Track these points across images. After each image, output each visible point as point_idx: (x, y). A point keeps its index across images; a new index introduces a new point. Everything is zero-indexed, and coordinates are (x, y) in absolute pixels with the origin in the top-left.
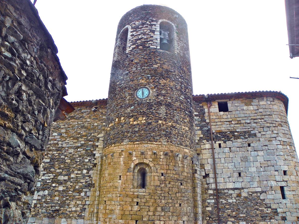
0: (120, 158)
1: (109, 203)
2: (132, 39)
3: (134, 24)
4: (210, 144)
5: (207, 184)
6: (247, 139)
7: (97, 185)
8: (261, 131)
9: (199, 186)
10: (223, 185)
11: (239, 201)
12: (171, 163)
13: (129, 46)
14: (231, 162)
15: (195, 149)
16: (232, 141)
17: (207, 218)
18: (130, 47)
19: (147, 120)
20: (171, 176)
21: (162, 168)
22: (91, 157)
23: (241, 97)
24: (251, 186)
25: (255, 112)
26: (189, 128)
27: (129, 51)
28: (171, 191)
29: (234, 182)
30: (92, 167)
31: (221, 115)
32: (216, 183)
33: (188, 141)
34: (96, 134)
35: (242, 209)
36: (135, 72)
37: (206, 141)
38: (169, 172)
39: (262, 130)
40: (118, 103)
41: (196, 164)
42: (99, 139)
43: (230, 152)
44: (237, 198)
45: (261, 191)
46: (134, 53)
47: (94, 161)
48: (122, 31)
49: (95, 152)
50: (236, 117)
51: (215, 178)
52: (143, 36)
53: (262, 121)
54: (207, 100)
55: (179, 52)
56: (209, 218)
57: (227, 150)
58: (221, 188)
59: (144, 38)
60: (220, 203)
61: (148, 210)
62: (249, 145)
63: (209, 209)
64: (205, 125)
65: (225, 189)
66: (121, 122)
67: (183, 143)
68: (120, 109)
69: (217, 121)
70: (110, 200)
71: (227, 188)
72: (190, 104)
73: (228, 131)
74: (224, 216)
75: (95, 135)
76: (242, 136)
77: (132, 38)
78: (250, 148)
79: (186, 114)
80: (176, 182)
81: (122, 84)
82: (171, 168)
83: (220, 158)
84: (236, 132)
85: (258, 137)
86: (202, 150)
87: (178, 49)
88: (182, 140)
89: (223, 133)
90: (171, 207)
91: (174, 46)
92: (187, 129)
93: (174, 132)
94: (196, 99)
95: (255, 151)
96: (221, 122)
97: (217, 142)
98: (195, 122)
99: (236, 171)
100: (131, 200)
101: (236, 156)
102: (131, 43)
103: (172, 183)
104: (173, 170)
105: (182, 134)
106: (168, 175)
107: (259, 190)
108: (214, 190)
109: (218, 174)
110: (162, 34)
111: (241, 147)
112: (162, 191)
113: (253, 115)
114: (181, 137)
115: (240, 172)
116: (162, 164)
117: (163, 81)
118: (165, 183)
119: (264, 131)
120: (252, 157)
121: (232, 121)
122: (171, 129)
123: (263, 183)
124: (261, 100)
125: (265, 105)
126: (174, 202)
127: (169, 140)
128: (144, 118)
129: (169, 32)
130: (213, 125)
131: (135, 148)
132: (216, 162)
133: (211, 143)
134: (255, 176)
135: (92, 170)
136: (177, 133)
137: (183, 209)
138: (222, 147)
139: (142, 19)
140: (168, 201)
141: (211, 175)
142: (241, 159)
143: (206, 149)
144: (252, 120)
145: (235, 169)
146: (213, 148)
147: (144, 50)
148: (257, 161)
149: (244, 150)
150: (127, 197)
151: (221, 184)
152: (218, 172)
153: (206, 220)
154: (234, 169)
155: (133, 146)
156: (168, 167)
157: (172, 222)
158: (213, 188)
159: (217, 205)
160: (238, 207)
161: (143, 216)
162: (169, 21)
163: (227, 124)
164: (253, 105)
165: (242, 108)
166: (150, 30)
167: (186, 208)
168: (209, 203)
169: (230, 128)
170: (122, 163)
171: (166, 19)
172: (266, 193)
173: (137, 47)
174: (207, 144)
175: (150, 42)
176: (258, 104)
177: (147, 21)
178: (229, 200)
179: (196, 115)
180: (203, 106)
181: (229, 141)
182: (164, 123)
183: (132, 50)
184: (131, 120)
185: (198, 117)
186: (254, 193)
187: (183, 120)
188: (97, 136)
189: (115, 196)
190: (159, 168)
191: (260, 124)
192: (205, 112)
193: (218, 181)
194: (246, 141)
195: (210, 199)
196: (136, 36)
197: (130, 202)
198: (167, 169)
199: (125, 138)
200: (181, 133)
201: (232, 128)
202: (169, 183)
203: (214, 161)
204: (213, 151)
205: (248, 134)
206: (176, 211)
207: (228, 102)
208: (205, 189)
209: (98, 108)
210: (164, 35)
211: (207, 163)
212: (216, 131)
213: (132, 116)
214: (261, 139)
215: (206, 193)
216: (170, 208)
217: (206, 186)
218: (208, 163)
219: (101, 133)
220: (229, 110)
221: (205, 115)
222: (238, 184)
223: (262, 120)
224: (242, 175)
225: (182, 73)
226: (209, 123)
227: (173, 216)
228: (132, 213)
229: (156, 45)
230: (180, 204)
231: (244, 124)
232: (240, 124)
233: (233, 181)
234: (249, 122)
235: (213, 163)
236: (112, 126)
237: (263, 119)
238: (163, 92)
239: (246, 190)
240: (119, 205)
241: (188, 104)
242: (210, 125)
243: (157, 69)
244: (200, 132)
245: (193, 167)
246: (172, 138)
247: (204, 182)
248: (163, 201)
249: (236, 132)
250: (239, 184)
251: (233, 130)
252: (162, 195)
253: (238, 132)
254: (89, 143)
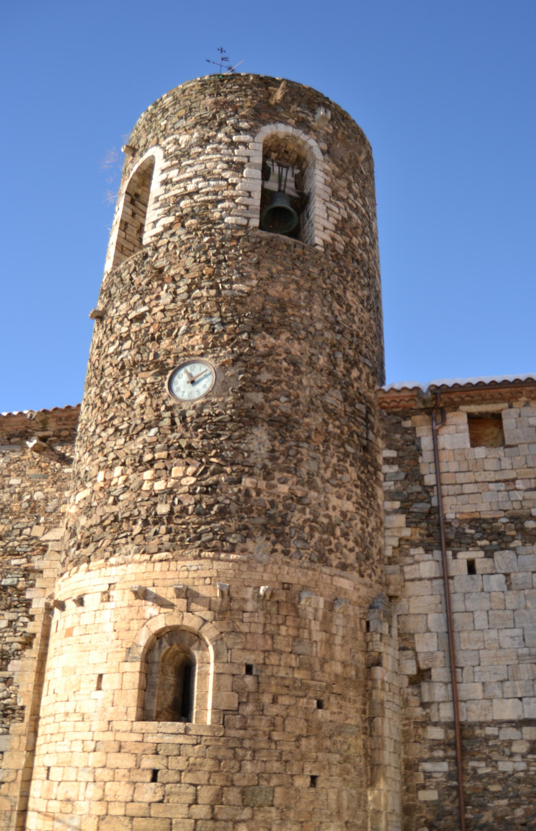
4: (438, 561)
5: (424, 705)
7: (27, 712)
9: (388, 713)
10: (479, 707)
14: (508, 626)
16: (514, 549)
18: (155, 222)
19: (202, 473)
20: (282, 673)
21: (248, 646)
22: (17, 610)
26: (359, 503)
28: (280, 728)
29: (520, 699)
30: (19, 646)
31: (477, 457)
32: (455, 701)
33: (351, 550)
34: (37, 531)
37: (421, 550)
38: (274, 659)
40: (109, 418)
41: (381, 634)
42: (46, 546)
46: (169, 242)
47: (25, 625)
54: (429, 405)
58: (473, 718)
61: (190, 799)
65: (489, 724)
68: (112, 438)
69: (464, 481)
72: (366, 420)
73: (502, 514)
74: (484, 820)
75: (33, 534)
79: (347, 454)
81: (125, 350)
82: (281, 644)
83: (472, 612)
86: (408, 584)
87: (325, 228)
89: (485, 521)
90: (278, 790)
92: (349, 506)
93: (297, 518)
96: (476, 482)
97: (460, 555)
98: (385, 484)
104: (291, 653)
106: (268, 671)
114: (325, 536)
118: (258, 701)
127: (279, 547)
128: (191, 470)
129: (298, 168)
131: (153, 576)
132: (457, 627)
136: (309, 520)
137: (323, 798)
138: (477, 572)
139: (202, 122)
140: (268, 765)
143: (420, 579)
145: (525, 651)
147: (203, 231)
150: (119, 751)
151: (473, 706)
152: (461, 662)
154: (520, 651)
155: (150, 566)
156: (270, 642)
159: (457, 780)
161: (174, 822)
163: (498, 491)
167: (336, 790)
168: (428, 775)
169: (507, 506)
173: (182, 220)
175: (226, 204)
177: (217, 131)
179: (388, 461)
180: (414, 429)
181: (502, 549)
182: (262, 484)
184: (148, 475)
185: (395, 468)
187: (333, 476)
188: (43, 539)
189: (80, 749)
190: (236, 647)
193: (462, 694)
196: (178, 182)
197: (130, 770)
198: (268, 647)
199: (123, 541)
200: (325, 521)
201: (517, 505)
202: (274, 701)
203: (450, 622)
204: (446, 586)
208: (415, 723)
209: (51, 441)
210: (280, 182)
211: (424, 629)
213: (152, 463)
216: (274, 791)
217: (419, 711)
218: (428, 631)
219: (56, 527)
221: (420, 460)
225: (339, 311)
228: (133, 812)
230: (314, 779)
235: (444, 629)
238: (265, 377)
240: (91, 779)
241: (359, 419)
243: (246, 298)
244: (400, 520)
245: (367, 643)
247: (411, 698)
248: (248, 767)
251: (521, 511)
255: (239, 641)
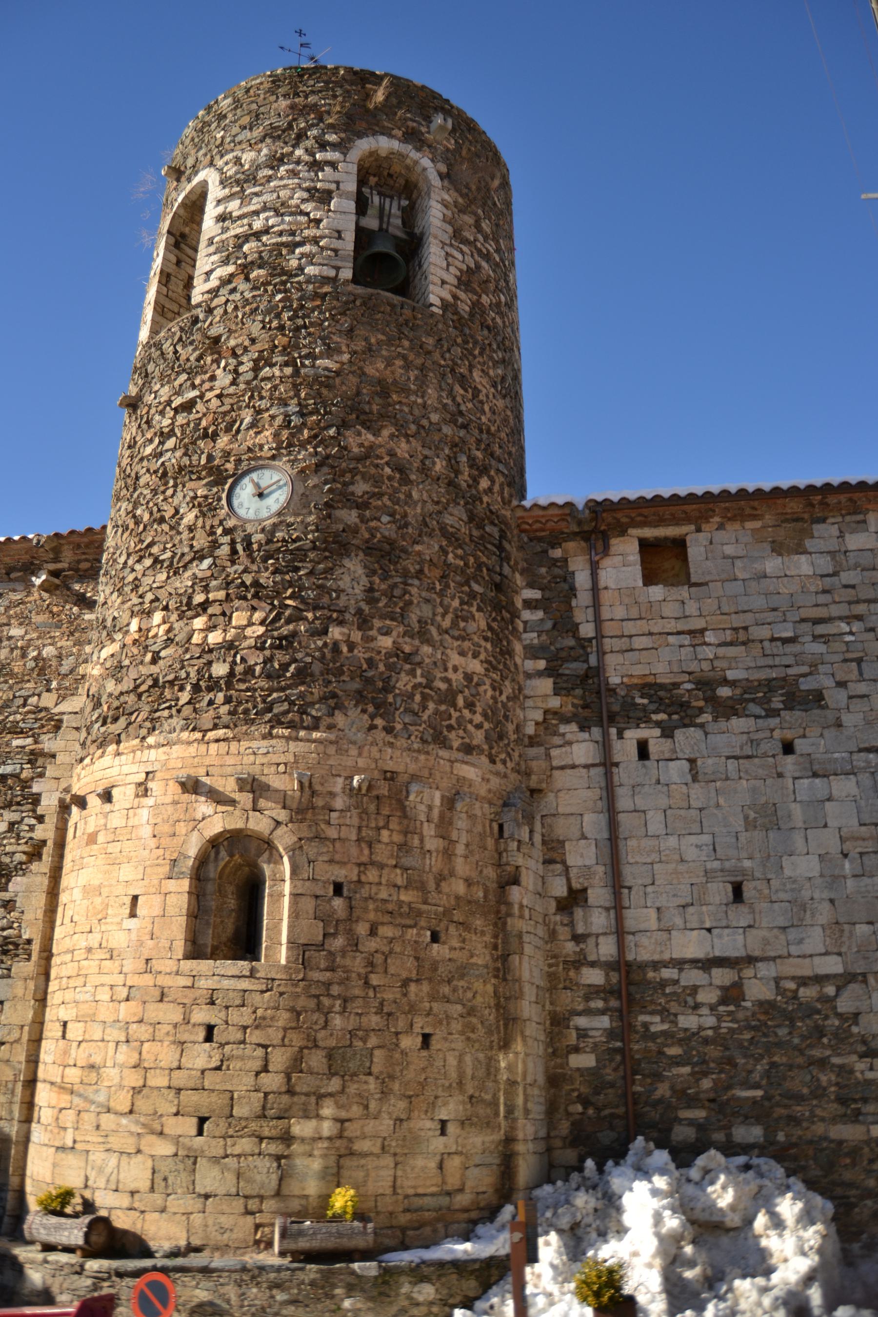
0: (139, 811)
1: (81, 1032)
2: (224, 236)
3: (238, 161)
4: (597, 742)
5: (577, 938)
6: (779, 715)
8: (846, 679)
10: (653, 941)
11: (730, 1025)
12: (385, 833)
13: (208, 268)
15: (518, 764)
16: (702, 726)
17: (571, 1109)
18: (208, 274)
19: (274, 621)
20: (383, 895)
21: (337, 857)
22: (20, 808)
23: (755, 512)
24: (794, 950)
25: (820, 584)
27: (203, 294)
28: (380, 969)
29: (709, 930)
30: (24, 858)
31: (652, 599)
32: (620, 932)
33: (479, 727)
34: (48, 700)
35: (746, 1064)
36: (225, 392)
37: (574, 727)
39: (855, 675)
40: (145, 544)
41: (519, 841)
42: (61, 721)
43: (695, 779)
44: (721, 1008)
45: (841, 975)
47: (32, 828)
48: (180, 199)
49: (42, 784)
50: (725, 609)
51: (618, 908)
52: (271, 217)
53: (854, 630)
55: (449, 298)
56: (579, 1108)
57: (677, 771)
58: (644, 956)
59: (276, 229)
60: (637, 1032)
61: (257, 1065)
62: (788, 748)
63: (585, 1061)
64: (572, 648)
65: (665, 964)
66: (151, 634)
67: (452, 735)
69: (633, 633)
70: (83, 1016)
71: (674, 956)
73: (686, 677)
74: (658, 1094)
76: (753, 700)
77: (223, 228)
78: (790, 759)
79: (473, 595)
80: (410, 927)
81: (167, 451)
82: (382, 854)
83: (644, 812)
84: (725, 682)
85: (831, 704)
86: (556, 773)
87: (443, 282)
88: (448, 722)
89: (662, 687)
90: (377, 1052)
91: (425, 266)
92: (476, 666)
94: (534, 527)
95: (815, 775)
96: (651, 634)
97: (628, 734)
98: (525, 636)
99: (719, 874)
100: (178, 1017)
101: (721, 801)
102: (215, 258)
103: (386, 931)
104: (396, 866)
105: (450, 689)
107: (833, 966)
108: (610, 966)
109: (630, 888)
110: (369, 212)
111: (748, 757)
112: (332, 969)
113: (813, 600)
114: (443, 708)
115: (739, 879)
116: (336, 836)
117: (359, 434)
118: (350, 932)
119: (866, 676)
120: (798, 805)
121: (705, 629)
122: (390, 667)
123: (851, 932)
124: (854, 525)
125: (871, 550)
126: (395, 1026)
127: (379, 722)
128: (258, 616)
130: (612, 652)
131: (207, 761)
132: (623, 832)
133: (600, 739)
134: (812, 899)
135: (21, 872)
138: (651, 757)
140: (364, 1019)
141: (598, 895)
142: (746, 818)
143: (573, 767)
144: (806, 627)
145: (716, 865)
146: (608, 764)
147: (275, 285)
148: (825, 826)
149: (761, 772)
150: (161, 1001)
151: (644, 940)
153: (569, 1114)
154: (709, 865)
155: (203, 748)
156: (366, 852)
157: (381, 1124)
158: (603, 959)
159: (622, 1041)
160: (727, 1053)
161: (236, 1096)
162: (408, 149)
163: (681, 646)
164: (810, 553)
165: (758, 566)
166: (308, 190)
167: (457, 1053)
168: (583, 1033)
169: (693, 666)
170: (146, 832)
171: (391, 136)
172: (865, 981)
174: (577, 741)
175: (307, 248)
176: (839, 543)
177: (295, 146)
178: (681, 1018)
179: (529, 604)
180: (565, 560)
181: (685, 726)
183: (218, 291)
184: (199, 623)
185: (540, 614)
186: (805, 984)
188: (56, 710)
189: (107, 997)
190: (320, 859)
191: (847, 643)
192: (577, 585)
193: (630, 923)
194: (772, 726)
195: (588, 1012)
196: (240, 218)
197: (175, 1026)
198: (364, 859)
199: (166, 713)
200: (443, 686)
201: (706, 666)
202: (373, 932)
203: (613, 825)
204: (608, 776)
205: (782, 695)
206: (401, 1071)
207: (688, 538)
209: (65, 576)
210: (381, 218)
211: (578, 834)
212: (625, 680)
213: (204, 606)
214: (847, 719)
215: (571, 986)
216: (372, 1055)
217: (570, 947)
218: (584, 837)
219: (72, 695)
220: (694, 579)
221: (574, 603)
222: (726, 939)
223: (856, 626)
224: (748, 891)
226: (594, 641)
227: (385, 1093)
229: (334, 263)
230: (426, 1039)
231: (766, 644)
232: (744, 643)
233: (703, 922)
234: (789, 634)
235: (606, 835)
236: (112, 655)
237: (859, 618)
239: (766, 970)
240: (123, 1039)
241: (489, 546)
242: (598, 651)
243: (334, 378)
244: (546, 685)
245: (500, 854)
246: (392, 709)
247: (560, 929)
248: (337, 1021)
249: (725, 682)
250: (735, 940)
252: (335, 990)
253: (733, 684)
254: (16, 743)
255: (325, 850)
